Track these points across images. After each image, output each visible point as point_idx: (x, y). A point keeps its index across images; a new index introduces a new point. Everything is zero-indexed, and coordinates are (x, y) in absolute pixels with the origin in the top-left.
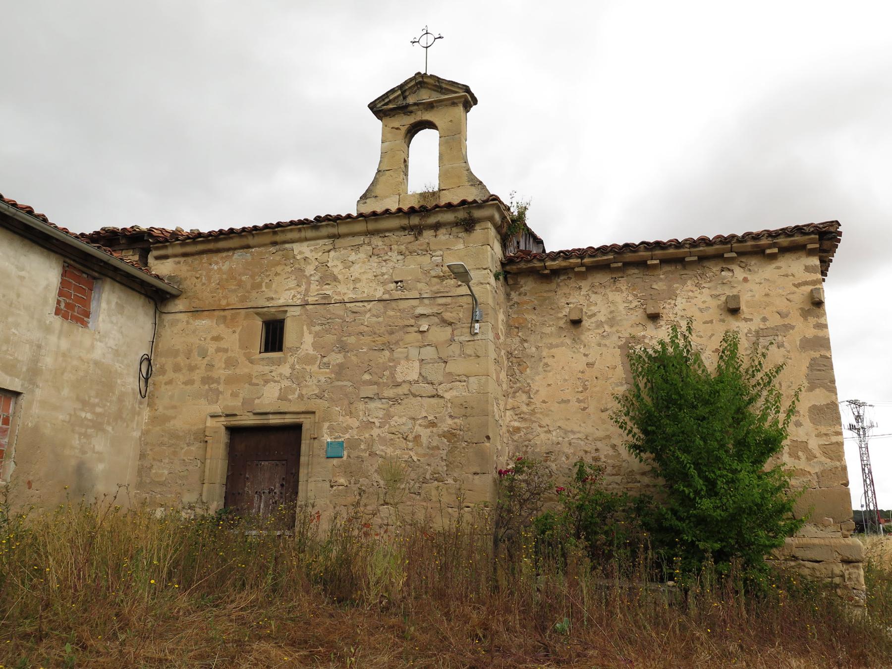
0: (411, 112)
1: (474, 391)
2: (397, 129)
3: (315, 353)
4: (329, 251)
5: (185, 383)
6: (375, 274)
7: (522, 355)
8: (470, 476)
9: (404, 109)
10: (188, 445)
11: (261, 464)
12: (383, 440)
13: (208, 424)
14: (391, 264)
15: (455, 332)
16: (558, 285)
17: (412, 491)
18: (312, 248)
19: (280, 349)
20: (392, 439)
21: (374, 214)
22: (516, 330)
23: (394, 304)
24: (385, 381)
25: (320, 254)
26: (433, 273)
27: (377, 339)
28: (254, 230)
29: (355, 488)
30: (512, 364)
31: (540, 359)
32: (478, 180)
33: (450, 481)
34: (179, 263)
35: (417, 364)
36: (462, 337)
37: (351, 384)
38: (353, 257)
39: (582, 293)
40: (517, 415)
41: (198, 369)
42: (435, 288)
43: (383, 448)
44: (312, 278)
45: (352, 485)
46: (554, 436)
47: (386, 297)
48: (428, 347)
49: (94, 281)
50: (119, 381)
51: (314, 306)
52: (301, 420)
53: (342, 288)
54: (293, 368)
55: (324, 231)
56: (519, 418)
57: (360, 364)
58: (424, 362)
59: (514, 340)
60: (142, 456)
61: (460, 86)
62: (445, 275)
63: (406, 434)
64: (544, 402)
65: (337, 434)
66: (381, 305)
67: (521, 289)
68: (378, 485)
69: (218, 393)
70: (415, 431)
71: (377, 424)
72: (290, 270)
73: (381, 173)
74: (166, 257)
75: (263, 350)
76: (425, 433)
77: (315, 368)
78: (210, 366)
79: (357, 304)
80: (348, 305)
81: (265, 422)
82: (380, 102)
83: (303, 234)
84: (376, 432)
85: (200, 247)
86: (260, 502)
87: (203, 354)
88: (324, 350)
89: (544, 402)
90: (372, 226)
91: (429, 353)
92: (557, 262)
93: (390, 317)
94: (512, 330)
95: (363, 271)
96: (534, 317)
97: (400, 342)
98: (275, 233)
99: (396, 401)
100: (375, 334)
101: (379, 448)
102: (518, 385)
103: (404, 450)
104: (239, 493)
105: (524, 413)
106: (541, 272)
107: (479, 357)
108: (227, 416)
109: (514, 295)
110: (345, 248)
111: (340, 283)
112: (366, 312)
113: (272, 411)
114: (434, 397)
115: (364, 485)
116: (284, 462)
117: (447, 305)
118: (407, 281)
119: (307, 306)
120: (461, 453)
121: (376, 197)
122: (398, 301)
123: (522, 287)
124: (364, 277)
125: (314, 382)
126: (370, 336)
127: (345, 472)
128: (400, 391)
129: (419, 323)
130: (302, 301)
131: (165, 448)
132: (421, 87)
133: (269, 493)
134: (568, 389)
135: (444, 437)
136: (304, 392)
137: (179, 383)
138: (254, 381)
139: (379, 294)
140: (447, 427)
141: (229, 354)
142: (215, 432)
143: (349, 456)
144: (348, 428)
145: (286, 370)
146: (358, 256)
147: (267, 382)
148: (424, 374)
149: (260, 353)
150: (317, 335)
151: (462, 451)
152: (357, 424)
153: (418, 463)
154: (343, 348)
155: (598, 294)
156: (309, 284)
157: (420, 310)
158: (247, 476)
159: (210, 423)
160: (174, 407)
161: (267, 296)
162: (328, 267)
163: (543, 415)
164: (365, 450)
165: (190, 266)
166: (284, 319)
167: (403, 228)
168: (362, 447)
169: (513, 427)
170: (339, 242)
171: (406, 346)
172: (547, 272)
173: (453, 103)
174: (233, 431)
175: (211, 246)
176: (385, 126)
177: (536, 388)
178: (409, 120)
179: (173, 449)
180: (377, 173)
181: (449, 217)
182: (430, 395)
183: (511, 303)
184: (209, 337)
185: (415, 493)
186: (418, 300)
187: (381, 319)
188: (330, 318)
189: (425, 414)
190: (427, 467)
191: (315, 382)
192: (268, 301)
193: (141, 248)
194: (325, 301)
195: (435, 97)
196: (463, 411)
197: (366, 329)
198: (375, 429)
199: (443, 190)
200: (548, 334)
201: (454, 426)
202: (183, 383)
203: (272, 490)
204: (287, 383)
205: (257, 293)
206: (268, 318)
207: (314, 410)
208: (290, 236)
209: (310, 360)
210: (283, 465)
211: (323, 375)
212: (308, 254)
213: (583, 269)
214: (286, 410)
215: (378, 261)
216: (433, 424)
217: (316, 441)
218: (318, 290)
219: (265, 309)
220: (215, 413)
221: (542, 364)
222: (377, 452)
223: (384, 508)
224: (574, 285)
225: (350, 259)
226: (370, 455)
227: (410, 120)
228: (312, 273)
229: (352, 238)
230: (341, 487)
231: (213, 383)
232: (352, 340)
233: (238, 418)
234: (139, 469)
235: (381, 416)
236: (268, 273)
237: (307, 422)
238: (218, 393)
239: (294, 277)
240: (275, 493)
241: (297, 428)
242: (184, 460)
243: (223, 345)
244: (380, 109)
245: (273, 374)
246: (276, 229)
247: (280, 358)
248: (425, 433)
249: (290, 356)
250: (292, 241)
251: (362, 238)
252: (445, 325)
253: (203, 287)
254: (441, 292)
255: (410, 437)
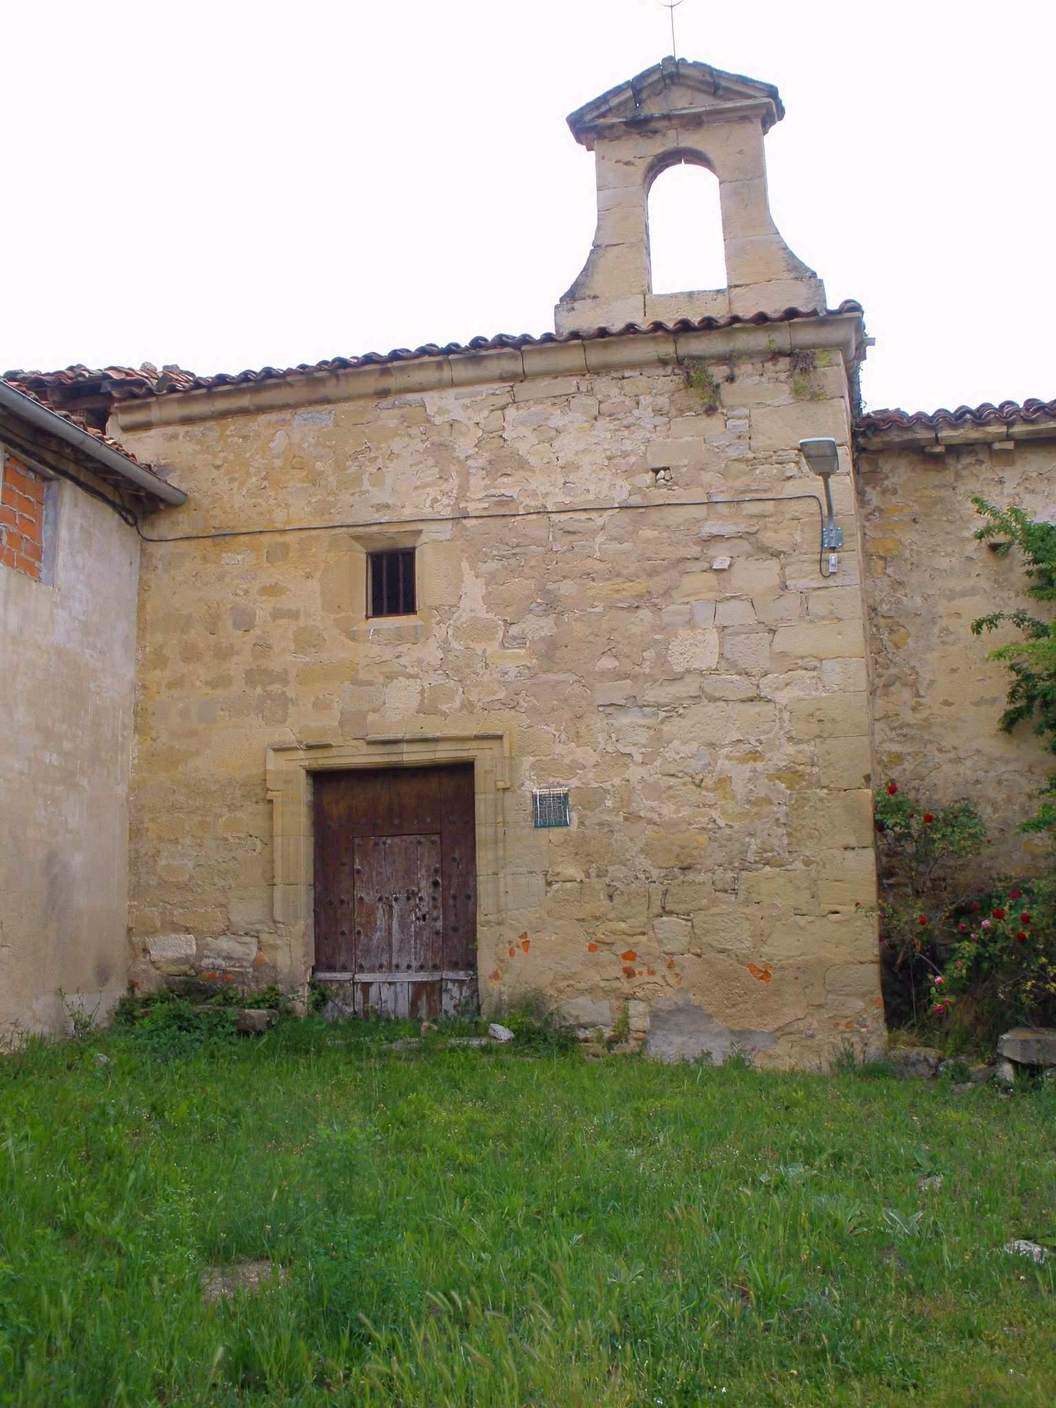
0: (655, 132)
1: (836, 688)
2: (628, 163)
3: (491, 615)
4: (503, 408)
5: (212, 684)
6: (609, 453)
7: (896, 612)
8: (838, 853)
9: (640, 126)
10: (231, 808)
11: (384, 843)
12: (653, 790)
13: (270, 767)
14: (640, 435)
15: (788, 571)
16: (958, 476)
17: (720, 887)
18: (467, 401)
19: (410, 608)
20: (670, 788)
21: (603, 333)
22: (881, 563)
23: (654, 515)
24: (647, 670)
25: (486, 413)
26: (733, 453)
27: (625, 586)
28: (340, 367)
29: (598, 884)
30: (878, 630)
31: (933, 621)
32: (807, 269)
33: (799, 865)
34: (174, 437)
35: (713, 637)
36: (805, 580)
37: (576, 678)
38: (558, 418)
39: (1006, 491)
40: (894, 729)
41: (237, 653)
42: (739, 484)
43: (654, 804)
44: (470, 462)
45: (595, 880)
46: (967, 769)
47: (636, 500)
48: (733, 602)
49: (45, 484)
50: (92, 686)
51: (480, 521)
52: (472, 753)
53: (538, 483)
54: (445, 647)
55: (493, 368)
56: (898, 735)
57: (591, 638)
58: (727, 631)
59: (878, 582)
60: (136, 832)
61: (757, 85)
62: (757, 455)
63: (701, 776)
64: (946, 703)
65: (551, 780)
66: (625, 517)
67: (886, 482)
68: (647, 878)
69: (285, 702)
70: (718, 769)
71: (638, 758)
72: (421, 447)
73: (601, 251)
74: (146, 426)
75: (370, 613)
76: (740, 774)
77: (492, 648)
78: (263, 648)
79: (576, 515)
80: (553, 516)
81: (394, 759)
82: (591, 111)
83: (446, 374)
84: (635, 773)
85: (221, 405)
86: (391, 917)
87: (245, 622)
88: (509, 609)
89: (946, 703)
90: (596, 356)
91: (736, 613)
92: (962, 431)
93: (648, 541)
94: (872, 564)
95: (581, 447)
96: (916, 538)
97: (673, 592)
98: (385, 372)
99: (672, 710)
100: (618, 575)
101: (644, 805)
102: (892, 671)
103: (698, 807)
104: (342, 902)
105: (908, 725)
106: (927, 449)
107: (840, 619)
108: (310, 748)
109: (873, 495)
110: (539, 401)
111: (534, 472)
112: (594, 533)
113: (408, 737)
114: (752, 701)
115: (619, 879)
116: (435, 838)
117: (765, 516)
118: (678, 467)
119: (464, 521)
120: (816, 809)
121: (595, 297)
122: (663, 508)
123: (887, 478)
124: (586, 460)
125: (495, 676)
126: (609, 579)
127: (577, 854)
128: (678, 689)
129: (711, 553)
130: (453, 511)
131: (181, 815)
132: (673, 83)
133: (408, 899)
134: (990, 678)
135: (779, 778)
136: (473, 697)
137: (198, 683)
138: (363, 676)
139: (621, 494)
140: (784, 760)
141: (302, 622)
142: (286, 782)
143: (582, 823)
144: (576, 767)
145: (431, 653)
146: (567, 419)
147: (390, 677)
148: (729, 655)
149: (367, 617)
150: (492, 579)
151: (819, 805)
152: (596, 758)
153: (728, 831)
154: (551, 605)
155: (1037, 493)
156: (465, 475)
157: (712, 528)
158: (357, 866)
159: (275, 763)
160: (192, 733)
161: (375, 501)
162: (505, 440)
163: (946, 729)
164: (615, 810)
165: (198, 443)
166: (414, 549)
167: (663, 362)
168: (609, 803)
169: (889, 753)
170: (523, 390)
171: (686, 600)
172: (939, 449)
173: (743, 117)
174: (321, 778)
175: (245, 401)
176: (600, 159)
177: (929, 676)
178: (656, 147)
179: (200, 819)
180: (592, 252)
181: (760, 340)
182: (744, 697)
183: (869, 509)
184: (255, 587)
185: (726, 891)
186: (705, 506)
187: (627, 546)
188: (518, 546)
189: (736, 736)
190: (747, 839)
191: (497, 676)
192: (378, 510)
193: (86, 409)
194: (503, 510)
195: (703, 104)
196: (815, 728)
197: (599, 566)
198: (633, 768)
199: (736, 286)
200: (946, 571)
201: (801, 758)
202: (207, 683)
203: (414, 894)
204: (437, 679)
205: (353, 494)
206: (380, 546)
207: (500, 733)
208: (418, 377)
209: (480, 630)
210: (433, 842)
211: (514, 661)
212: (457, 414)
213: (1010, 445)
214: (438, 734)
215: (612, 427)
216: (755, 755)
217: (508, 794)
218: (486, 488)
219: (375, 529)
220: (284, 743)
221: (936, 630)
222: (642, 814)
223: (663, 923)
224: (989, 475)
225: (552, 424)
226: (626, 819)
227: (656, 147)
228: (471, 452)
229: (553, 381)
230: (569, 885)
231: (272, 683)
232: (567, 588)
233: (334, 752)
234: (130, 858)
235: (644, 741)
236: (372, 455)
237: (485, 759)
238: (285, 702)
239: (431, 462)
240: (421, 899)
241: (464, 769)
242: (226, 839)
243: (286, 602)
244: (592, 124)
245: (402, 661)
246: (389, 365)
247: (416, 627)
248: (740, 774)
249: (438, 623)
250: (422, 389)
251: (574, 381)
252: (764, 556)
253: (232, 486)
254: (752, 491)
255: (708, 782)
